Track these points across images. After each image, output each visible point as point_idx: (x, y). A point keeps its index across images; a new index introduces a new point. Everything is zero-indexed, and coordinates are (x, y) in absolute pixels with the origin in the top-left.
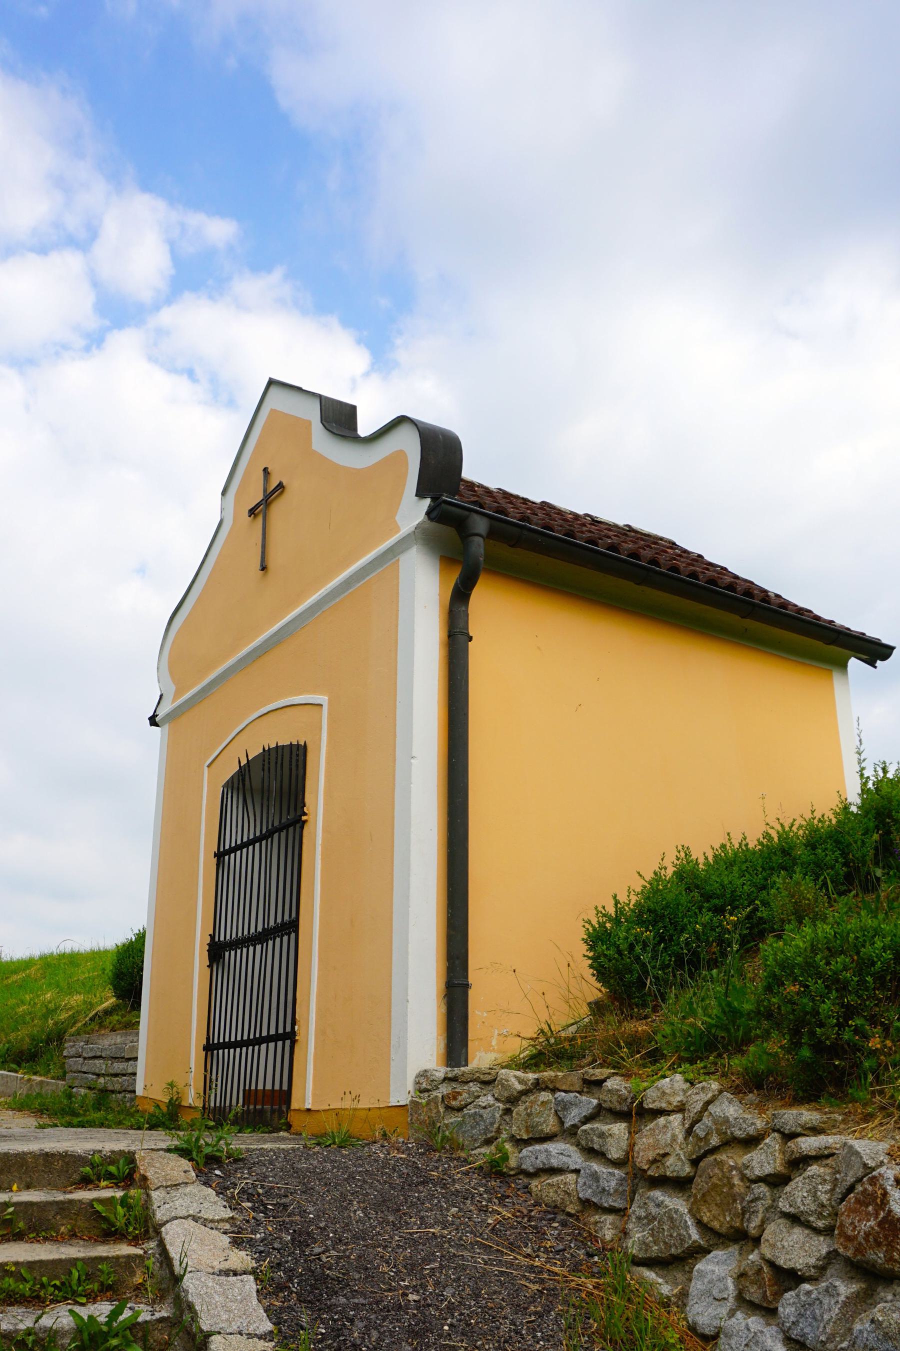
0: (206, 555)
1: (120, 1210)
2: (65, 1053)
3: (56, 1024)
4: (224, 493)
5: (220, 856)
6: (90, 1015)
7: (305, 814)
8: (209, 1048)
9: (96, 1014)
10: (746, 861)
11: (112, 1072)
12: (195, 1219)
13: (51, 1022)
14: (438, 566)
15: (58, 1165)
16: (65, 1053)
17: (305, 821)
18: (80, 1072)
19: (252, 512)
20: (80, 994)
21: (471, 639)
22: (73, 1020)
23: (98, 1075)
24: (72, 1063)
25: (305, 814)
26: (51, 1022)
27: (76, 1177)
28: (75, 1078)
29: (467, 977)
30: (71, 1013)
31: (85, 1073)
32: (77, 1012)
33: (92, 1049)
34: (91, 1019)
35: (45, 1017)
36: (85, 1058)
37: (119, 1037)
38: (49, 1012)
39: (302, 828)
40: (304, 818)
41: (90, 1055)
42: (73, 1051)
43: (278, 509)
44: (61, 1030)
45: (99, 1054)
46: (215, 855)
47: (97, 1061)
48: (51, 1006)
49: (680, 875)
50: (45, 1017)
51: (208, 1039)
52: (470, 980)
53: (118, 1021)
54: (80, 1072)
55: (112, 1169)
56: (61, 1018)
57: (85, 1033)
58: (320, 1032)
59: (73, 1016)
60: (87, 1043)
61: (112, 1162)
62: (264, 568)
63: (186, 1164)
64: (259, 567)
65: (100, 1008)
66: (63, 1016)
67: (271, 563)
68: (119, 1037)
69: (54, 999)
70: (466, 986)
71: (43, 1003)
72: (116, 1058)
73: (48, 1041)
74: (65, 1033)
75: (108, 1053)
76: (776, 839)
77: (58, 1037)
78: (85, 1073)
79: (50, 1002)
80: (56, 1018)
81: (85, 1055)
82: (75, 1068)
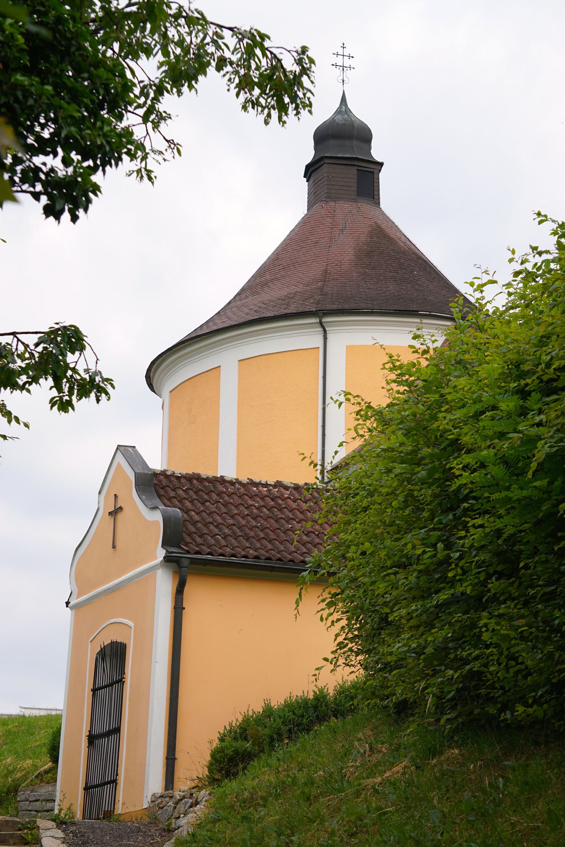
0: (92, 523)
1: (30, 836)
2: (18, 799)
3: (13, 781)
4: (100, 493)
5: (94, 690)
6: (36, 774)
7: (124, 678)
8: (86, 789)
9: (39, 773)
10: (340, 694)
11: (45, 809)
12: (52, 837)
13: (10, 779)
14: (172, 576)
15: (11, 824)
16: (18, 799)
17: (124, 682)
18: (27, 810)
19: (110, 513)
20: (30, 758)
21: (184, 608)
22: (24, 778)
23: (37, 811)
24: (22, 805)
25: (124, 678)
26: (10, 779)
27: (17, 828)
28: (24, 815)
29: (174, 754)
30: (23, 773)
31: (30, 811)
32: (28, 772)
33: (34, 796)
34: (36, 777)
35: (6, 776)
36: (30, 802)
37: (50, 787)
38: (9, 773)
39: (123, 684)
40: (123, 680)
41: (34, 799)
42: (23, 797)
43: (120, 516)
44: (16, 785)
45: (38, 798)
46: (92, 690)
47: (37, 803)
48: (11, 768)
49: (316, 698)
50: (6, 776)
51: (86, 784)
52: (176, 757)
53: (51, 777)
54: (27, 810)
55: (29, 826)
56: (17, 776)
57: (31, 785)
58: (125, 779)
59: (25, 775)
60: (32, 791)
61: (29, 824)
62: (114, 547)
63: (53, 823)
64: (111, 546)
65: (42, 769)
66: (19, 775)
67: (119, 544)
68: (50, 787)
69: (13, 763)
70: (175, 759)
71: (5, 766)
72: (48, 800)
73: (8, 792)
74: (19, 786)
75: (44, 797)
76: (318, 693)
77: (14, 790)
78: (30, 811)
79: (10, 765)
80: (13, 776)
81: (30, 799)
82: (24, 808)
